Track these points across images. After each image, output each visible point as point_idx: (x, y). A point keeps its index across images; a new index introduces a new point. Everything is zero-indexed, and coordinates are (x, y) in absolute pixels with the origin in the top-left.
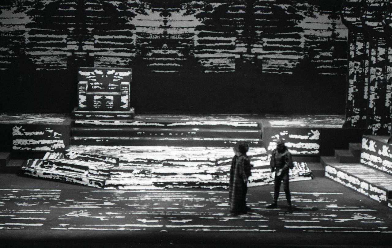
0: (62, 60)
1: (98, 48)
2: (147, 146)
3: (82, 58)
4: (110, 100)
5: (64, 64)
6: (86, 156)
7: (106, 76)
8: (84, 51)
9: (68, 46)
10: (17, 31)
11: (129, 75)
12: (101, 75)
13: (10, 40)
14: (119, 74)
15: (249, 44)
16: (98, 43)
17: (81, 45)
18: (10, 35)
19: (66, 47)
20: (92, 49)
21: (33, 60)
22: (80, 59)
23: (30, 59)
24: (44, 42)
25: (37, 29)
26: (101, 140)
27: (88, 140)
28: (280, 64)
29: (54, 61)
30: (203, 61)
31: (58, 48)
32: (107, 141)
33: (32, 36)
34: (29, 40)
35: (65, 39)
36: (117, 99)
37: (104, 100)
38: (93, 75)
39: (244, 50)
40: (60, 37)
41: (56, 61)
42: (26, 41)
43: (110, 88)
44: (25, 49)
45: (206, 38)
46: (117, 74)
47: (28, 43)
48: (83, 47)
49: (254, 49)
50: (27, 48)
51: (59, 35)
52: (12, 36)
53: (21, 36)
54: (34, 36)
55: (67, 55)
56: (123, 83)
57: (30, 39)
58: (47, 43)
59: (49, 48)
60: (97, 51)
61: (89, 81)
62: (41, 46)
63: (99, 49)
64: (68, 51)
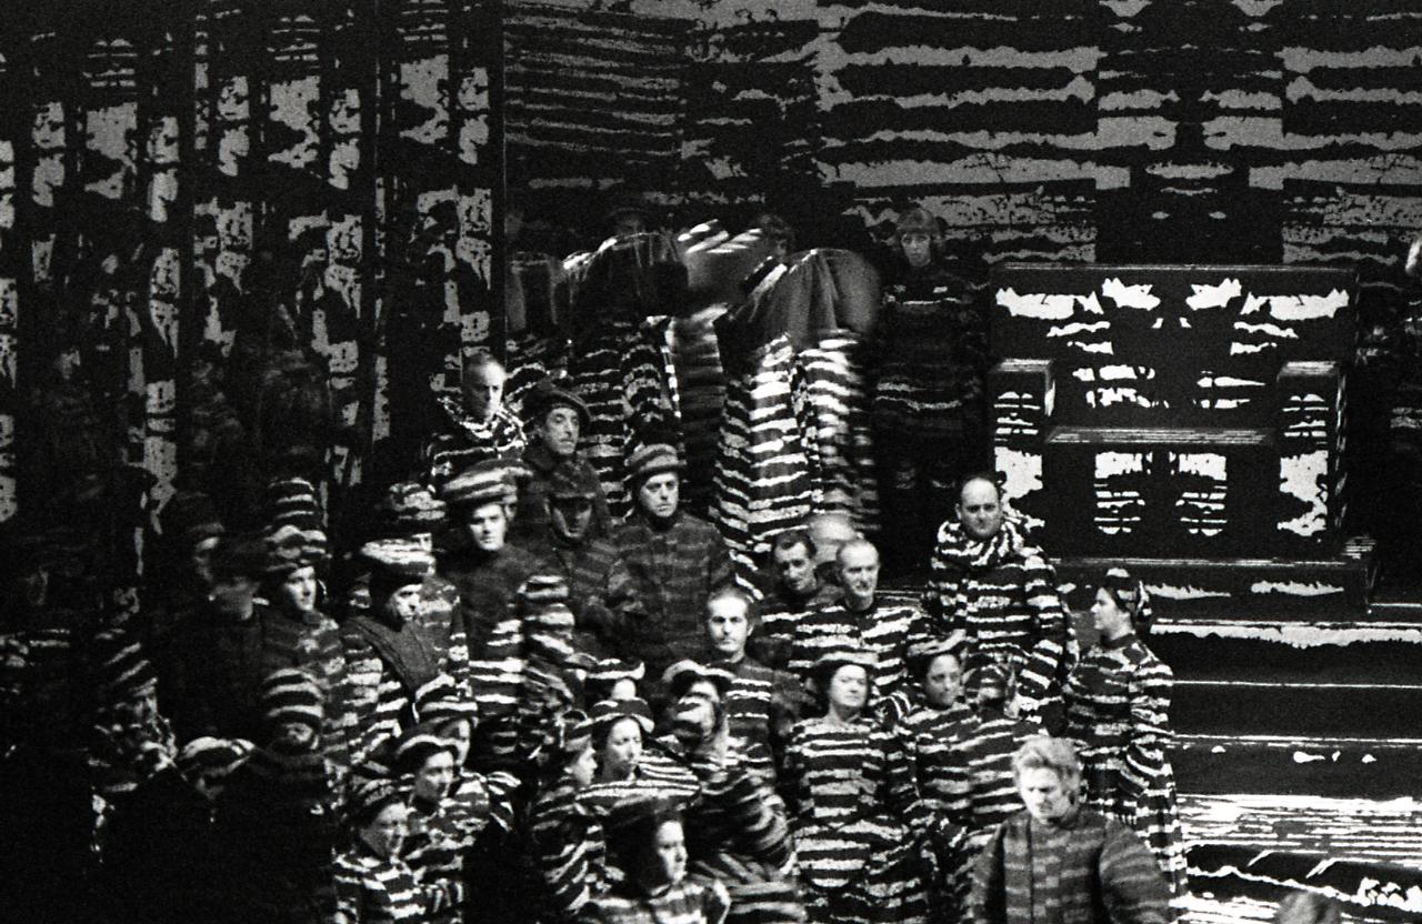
0: (1062, 221)
1: (1310, 132)
2: (1252, 793)
3: (1200, 207)
4: (1206, 484)
5: (1079, 244)
6: (1225, 871)
7: (1184, 323)
8: (1215, 157)
9: (1104, 123)
10: (766, 24)
11: (1339, 311)
12: (1145, 316)
13: (718, 86)
14: (1266, 307)
15: (1190, 92)
16: (1308, 99)
17: (1190, 117)
18: (713, 50)
19: (1095, 129)
20: (1268, 144)
21: (870, 221)
22: (1188, 210)
23: (849, 212)
24: (940, 100)
25: (896, 10)
26: (1328, 753)
27: (1236, 755)
28: (1402, 222)
29: (1013, 227)
30: (875, 210)
31: (1037, 138)
32: (1368, 759)
33: (860, 59)
34: (845, 85)
35: (1088, 75)
36: (1253, 475)
37: (1160, 480)
38: (1091, 318)
39: (1158, 133)
40: (1048, 60)
41: (1027, 227)
42: (822, 92)
43: (1206, 404)
44: (816, 145)
45: (901, 55)
46: (1252, 304)
47: (836, 108)
48: (1210, 127)
49: (1220, 123)
50: (833, 143)
51: (1047, 49)
52: (729, 57)
53: (787, 57)
54: (878, 59)
55: (1101, 186)
56: (1294, 367)
57: (847, 77)
58: (967, 104)
59: (978, 139)
60: (1299, 157)
61: (1065, 357)
62: (921, 128)
63: (1320, 141)
64: (1107, 157)
